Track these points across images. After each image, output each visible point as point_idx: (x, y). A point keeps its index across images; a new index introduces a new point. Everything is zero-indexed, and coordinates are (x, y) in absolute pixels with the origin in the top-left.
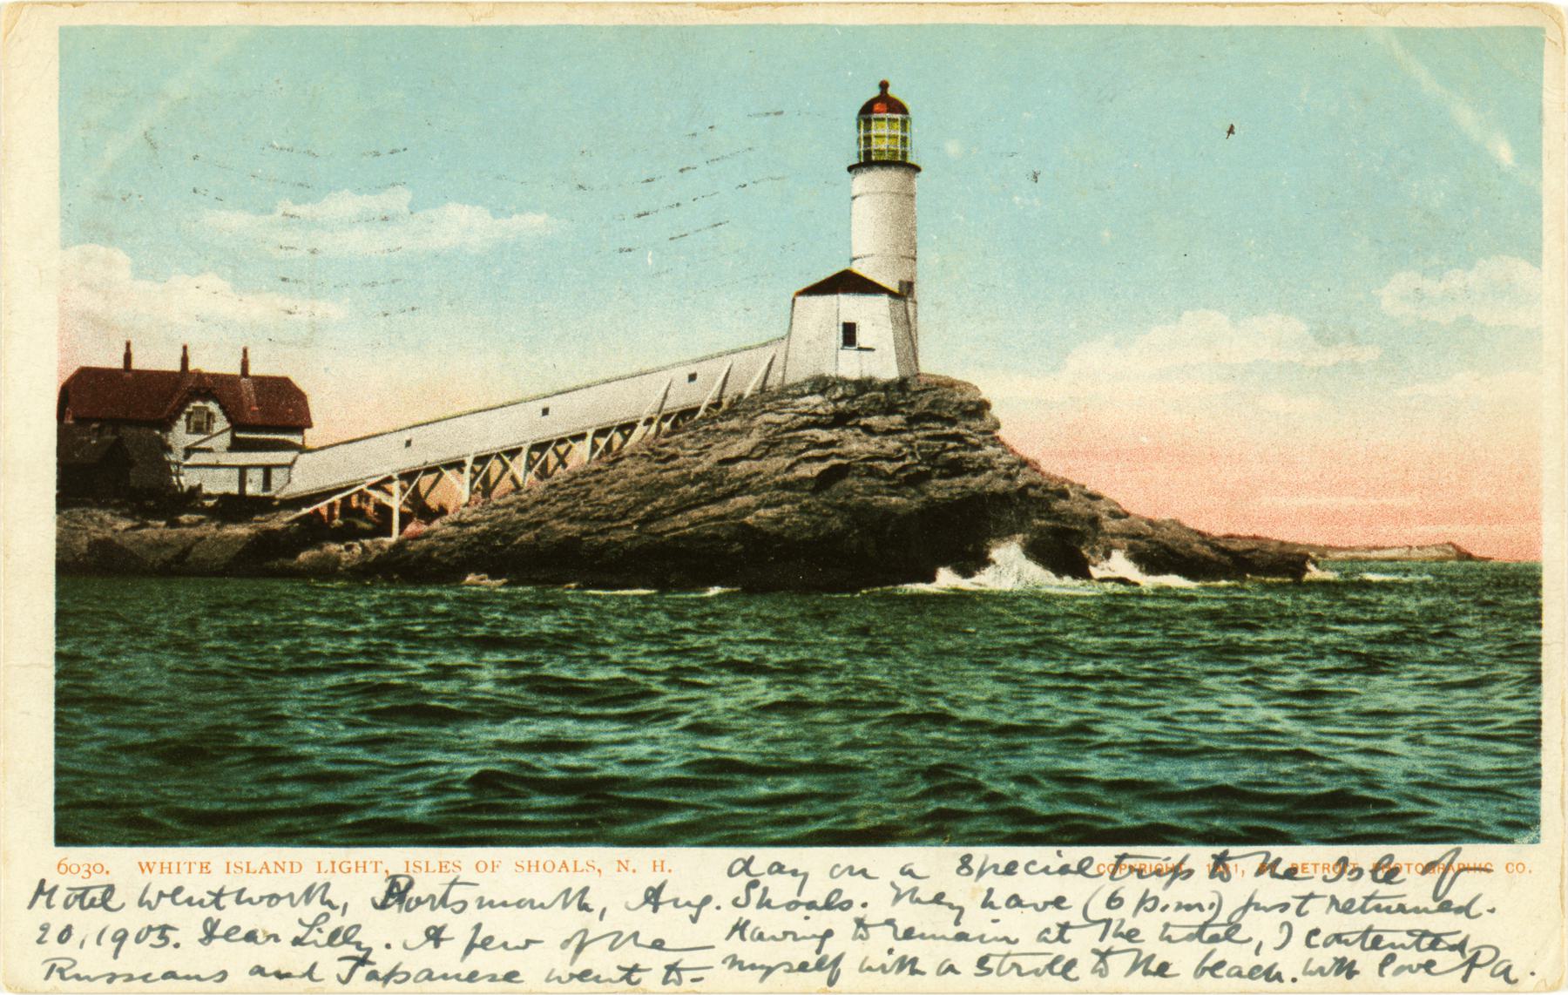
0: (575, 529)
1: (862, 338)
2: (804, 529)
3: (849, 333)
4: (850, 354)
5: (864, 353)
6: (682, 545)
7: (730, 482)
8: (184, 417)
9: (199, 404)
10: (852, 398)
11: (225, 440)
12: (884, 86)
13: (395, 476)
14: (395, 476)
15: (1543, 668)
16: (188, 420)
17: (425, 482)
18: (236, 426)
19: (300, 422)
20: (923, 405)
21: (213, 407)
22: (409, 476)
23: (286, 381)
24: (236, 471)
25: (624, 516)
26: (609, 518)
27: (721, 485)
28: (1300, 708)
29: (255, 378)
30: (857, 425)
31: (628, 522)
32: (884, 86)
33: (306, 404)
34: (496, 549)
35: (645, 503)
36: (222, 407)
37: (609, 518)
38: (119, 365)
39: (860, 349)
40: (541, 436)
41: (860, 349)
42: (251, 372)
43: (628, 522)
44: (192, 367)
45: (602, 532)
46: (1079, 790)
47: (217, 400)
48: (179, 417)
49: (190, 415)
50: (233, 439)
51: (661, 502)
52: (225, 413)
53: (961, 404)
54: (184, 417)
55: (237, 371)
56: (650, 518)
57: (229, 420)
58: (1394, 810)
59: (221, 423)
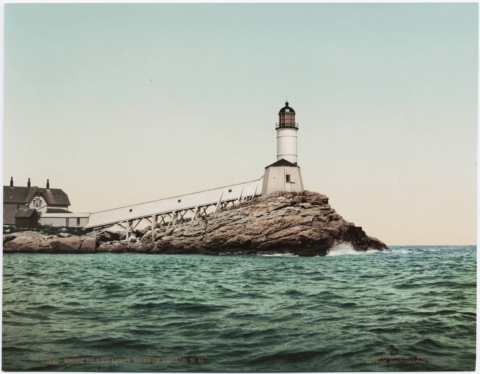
1: (292, 179)
3: (288, 178)
5: (292, 184)
8: (33, 202)
9: (37, 197)
10: (293, 198)
11: (45, 209)
12: (287, 104)
15: (2, 270)
16: (34, 203)
17: (135, 223)
18: (49, 205)
20: (314, 199)
21: (42, 198)
22: (131, 221)
23: (61, 190)
24: (76, 219)
25: (261, 233)
26: (258, 234)
27: (285, 224)
29: (51, 190)
31: (262, 235)
32: (287, 104)
35: (266, 229)
36: (44, 199)
38: (26, 186)
39: (291, 183)
40: (179, 208)
41: (291, 183)
43: (262, 235)
45: (257, 238)
46: (211, 317)
47: (43, 196)
48: (31, 202)
52: (46, 201)
53: (323, 199)
54: (33, 202)
57: (47, 203)
58: (445, 326)
59: (44, 203)
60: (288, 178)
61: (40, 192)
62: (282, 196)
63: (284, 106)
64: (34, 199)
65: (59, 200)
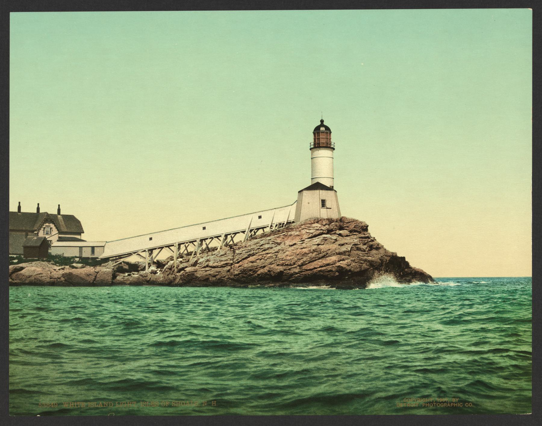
0: (281, 268)
1: (328, 204)
2: (357, 268)
3: (323, 203)
4: (324, 210)
5: (328, 210)
6: (321, 273)
7: (323, 252)
8: (42, 229)
9: (47, 224)
10: (329, 225)
11: (56, 237)
12: (322, 121)
13: (147, 250)
14: (147, 250)
16: (44, 230)
17: (155, 252)
18: (60, 232)
19: (80, 231)
20: (352, 227)
21: (52, 225)
22: (151, 251)
24: (90, 248)
25: (294, 264)
26: (291, 265)
28: (285, 327)
29: (62, 215)
30: (335, 233)
31: (295, 266)
32: (322, 121)
33: (81, 225)
34: (251, 275)
35: (300, 259)
36: (55, 226)
37: (291, 265)
42: (61, 213)
43: (295, 266)
44: (41, 211)
45: (289, 269)
46: (240, 356)
47: (54, 223)
49: (44, 228)
50: (59, 237)
51: (305, 259)
52: (57, 228)
54: (42, 229)
55: (56, 212)
56: (303, 265)
57: (58, 230)
59: (55, 231)
60: (323, 203)
61: (50, 219)
62: (317, 222)
63: (319, 123)
64: (44, 227)
65: (71, 227)
